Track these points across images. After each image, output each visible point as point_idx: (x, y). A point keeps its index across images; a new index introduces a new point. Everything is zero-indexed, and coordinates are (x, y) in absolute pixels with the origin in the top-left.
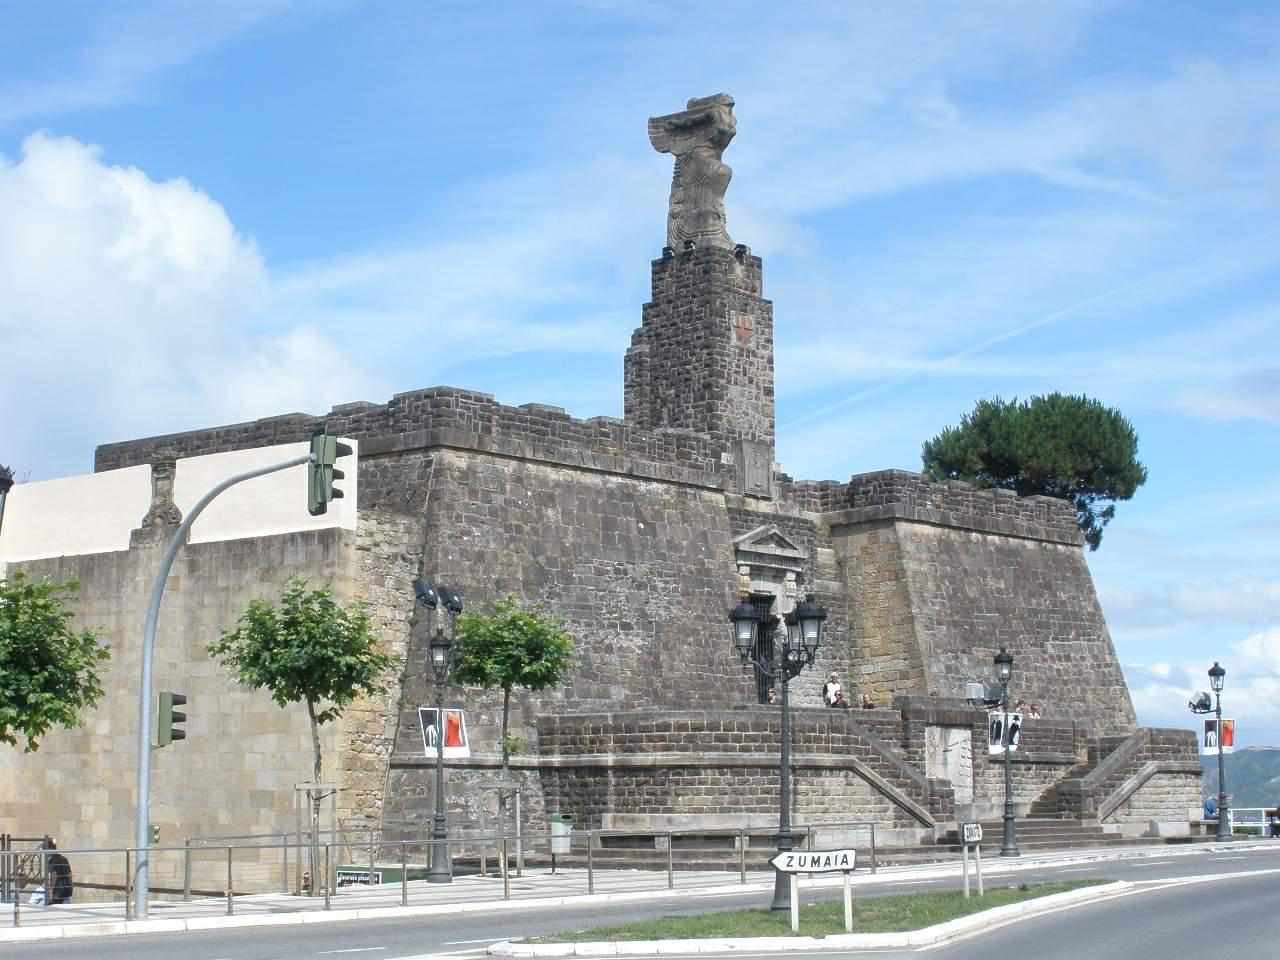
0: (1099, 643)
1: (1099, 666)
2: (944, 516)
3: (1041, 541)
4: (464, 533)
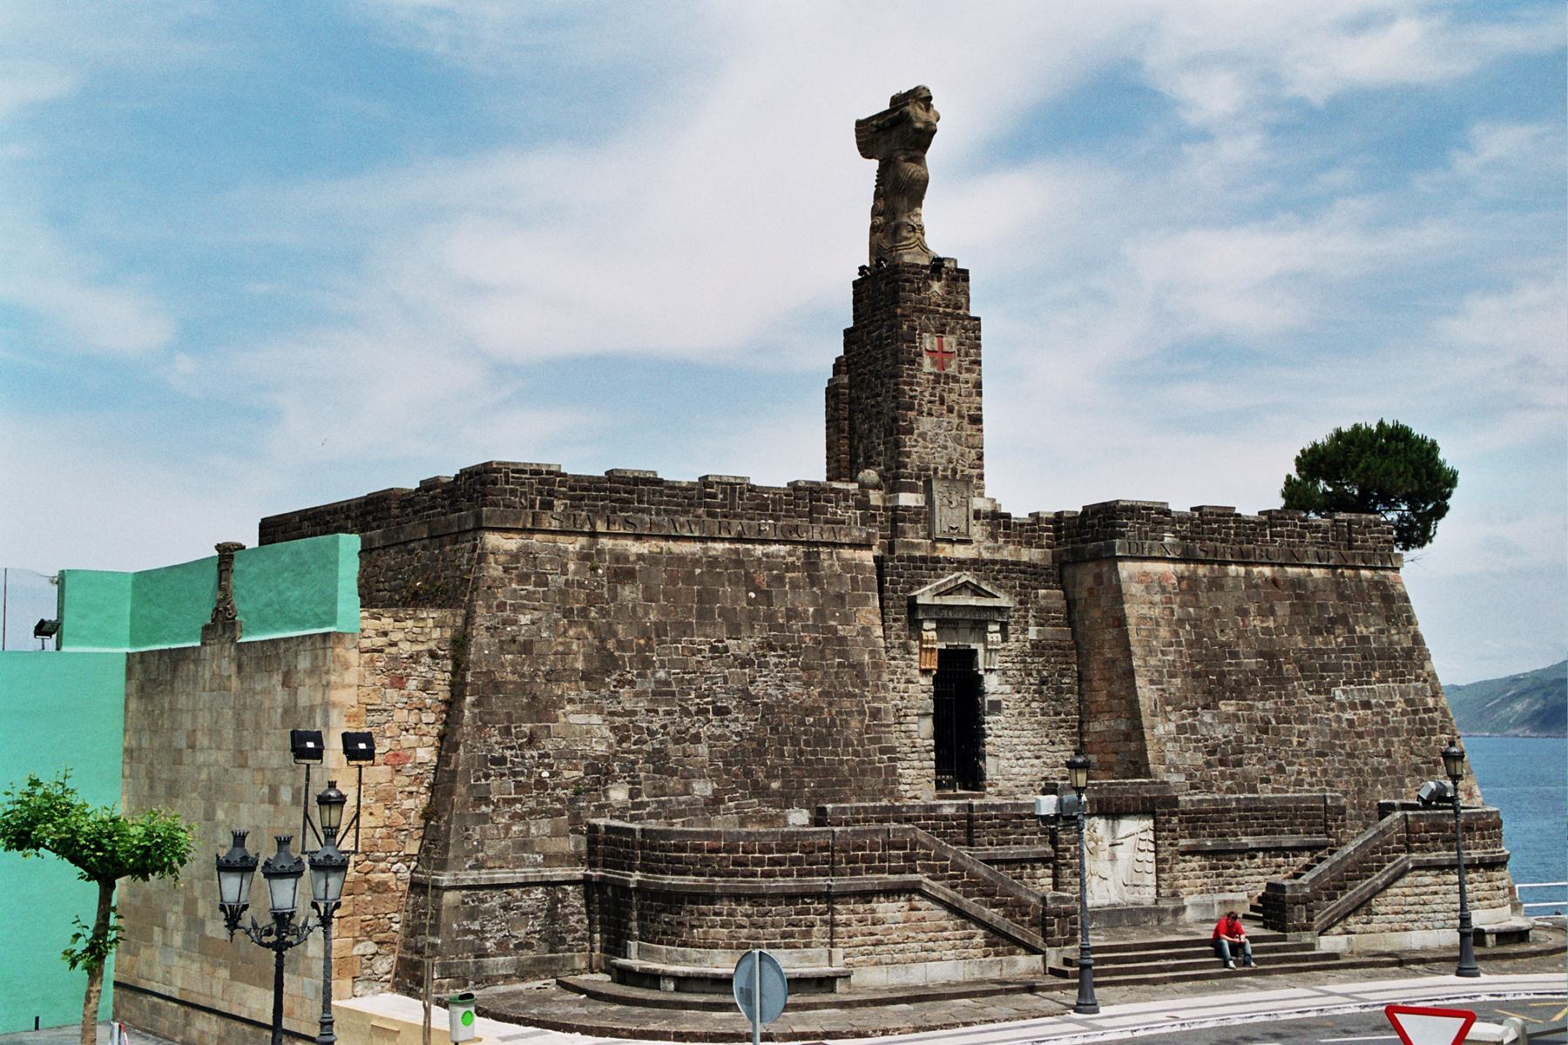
0: (1420, 684)
1: (1415, 712)
2: (1186, 550)
3: (1335, 567)
4: (505, 622)
